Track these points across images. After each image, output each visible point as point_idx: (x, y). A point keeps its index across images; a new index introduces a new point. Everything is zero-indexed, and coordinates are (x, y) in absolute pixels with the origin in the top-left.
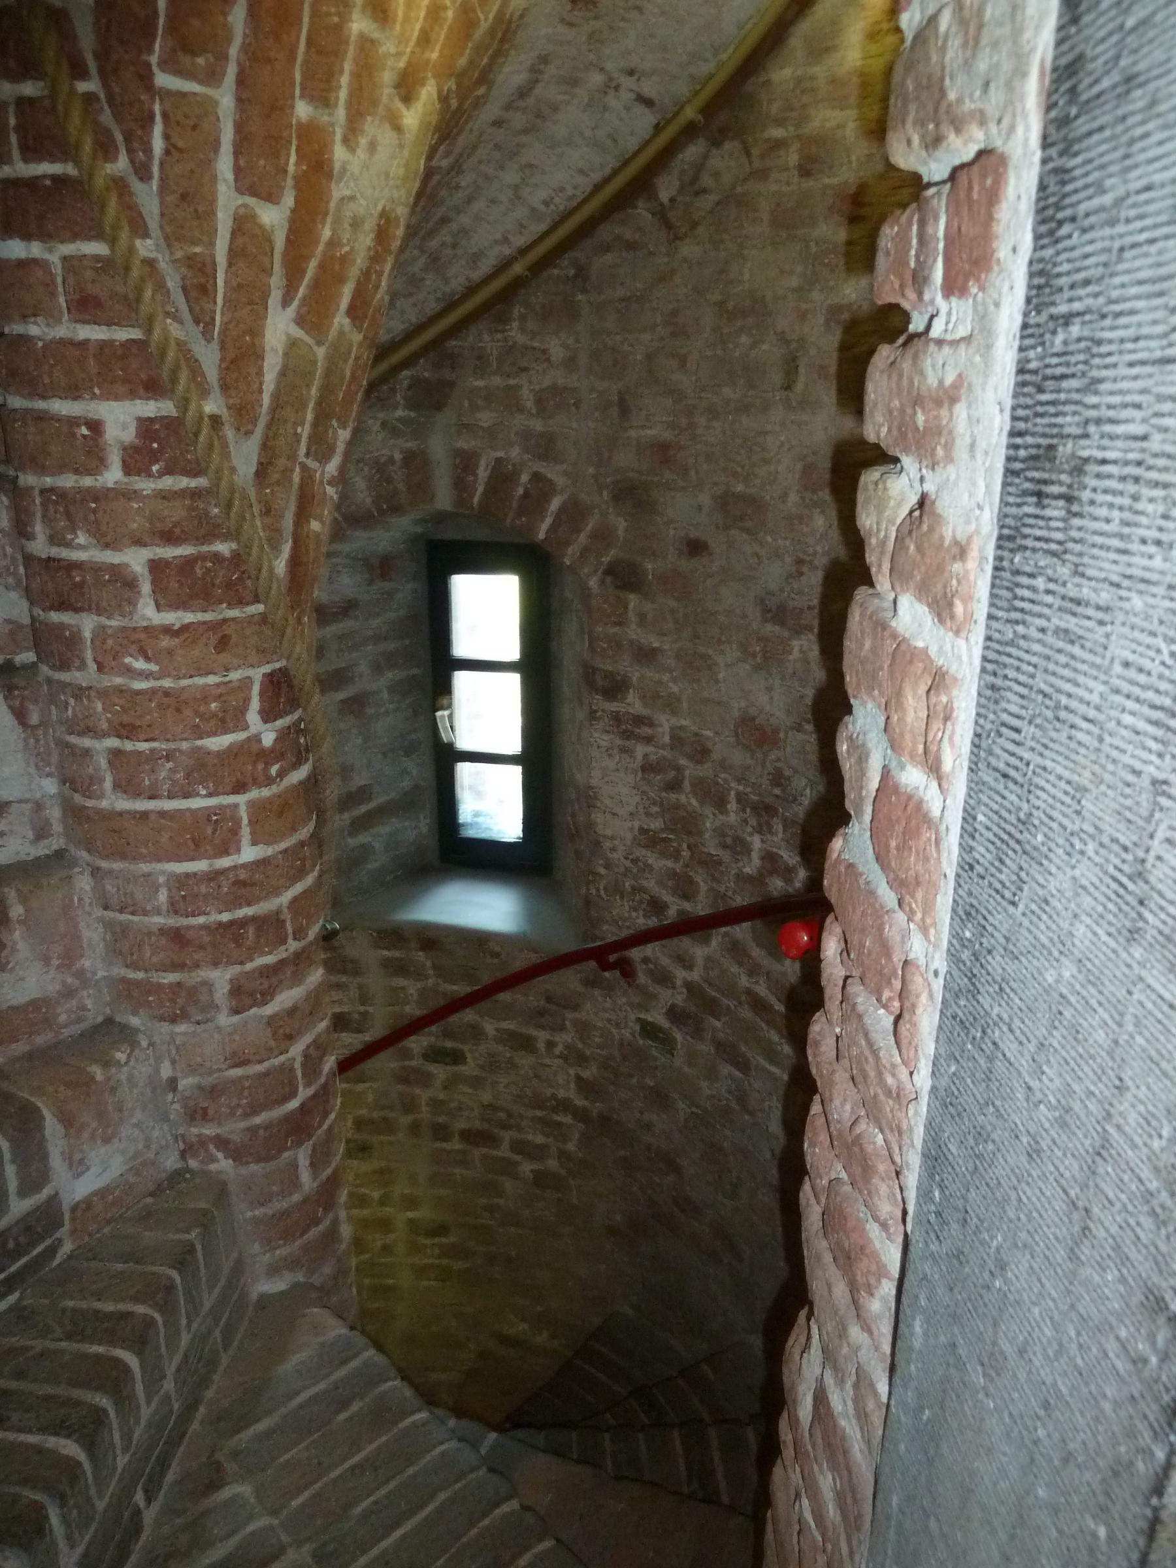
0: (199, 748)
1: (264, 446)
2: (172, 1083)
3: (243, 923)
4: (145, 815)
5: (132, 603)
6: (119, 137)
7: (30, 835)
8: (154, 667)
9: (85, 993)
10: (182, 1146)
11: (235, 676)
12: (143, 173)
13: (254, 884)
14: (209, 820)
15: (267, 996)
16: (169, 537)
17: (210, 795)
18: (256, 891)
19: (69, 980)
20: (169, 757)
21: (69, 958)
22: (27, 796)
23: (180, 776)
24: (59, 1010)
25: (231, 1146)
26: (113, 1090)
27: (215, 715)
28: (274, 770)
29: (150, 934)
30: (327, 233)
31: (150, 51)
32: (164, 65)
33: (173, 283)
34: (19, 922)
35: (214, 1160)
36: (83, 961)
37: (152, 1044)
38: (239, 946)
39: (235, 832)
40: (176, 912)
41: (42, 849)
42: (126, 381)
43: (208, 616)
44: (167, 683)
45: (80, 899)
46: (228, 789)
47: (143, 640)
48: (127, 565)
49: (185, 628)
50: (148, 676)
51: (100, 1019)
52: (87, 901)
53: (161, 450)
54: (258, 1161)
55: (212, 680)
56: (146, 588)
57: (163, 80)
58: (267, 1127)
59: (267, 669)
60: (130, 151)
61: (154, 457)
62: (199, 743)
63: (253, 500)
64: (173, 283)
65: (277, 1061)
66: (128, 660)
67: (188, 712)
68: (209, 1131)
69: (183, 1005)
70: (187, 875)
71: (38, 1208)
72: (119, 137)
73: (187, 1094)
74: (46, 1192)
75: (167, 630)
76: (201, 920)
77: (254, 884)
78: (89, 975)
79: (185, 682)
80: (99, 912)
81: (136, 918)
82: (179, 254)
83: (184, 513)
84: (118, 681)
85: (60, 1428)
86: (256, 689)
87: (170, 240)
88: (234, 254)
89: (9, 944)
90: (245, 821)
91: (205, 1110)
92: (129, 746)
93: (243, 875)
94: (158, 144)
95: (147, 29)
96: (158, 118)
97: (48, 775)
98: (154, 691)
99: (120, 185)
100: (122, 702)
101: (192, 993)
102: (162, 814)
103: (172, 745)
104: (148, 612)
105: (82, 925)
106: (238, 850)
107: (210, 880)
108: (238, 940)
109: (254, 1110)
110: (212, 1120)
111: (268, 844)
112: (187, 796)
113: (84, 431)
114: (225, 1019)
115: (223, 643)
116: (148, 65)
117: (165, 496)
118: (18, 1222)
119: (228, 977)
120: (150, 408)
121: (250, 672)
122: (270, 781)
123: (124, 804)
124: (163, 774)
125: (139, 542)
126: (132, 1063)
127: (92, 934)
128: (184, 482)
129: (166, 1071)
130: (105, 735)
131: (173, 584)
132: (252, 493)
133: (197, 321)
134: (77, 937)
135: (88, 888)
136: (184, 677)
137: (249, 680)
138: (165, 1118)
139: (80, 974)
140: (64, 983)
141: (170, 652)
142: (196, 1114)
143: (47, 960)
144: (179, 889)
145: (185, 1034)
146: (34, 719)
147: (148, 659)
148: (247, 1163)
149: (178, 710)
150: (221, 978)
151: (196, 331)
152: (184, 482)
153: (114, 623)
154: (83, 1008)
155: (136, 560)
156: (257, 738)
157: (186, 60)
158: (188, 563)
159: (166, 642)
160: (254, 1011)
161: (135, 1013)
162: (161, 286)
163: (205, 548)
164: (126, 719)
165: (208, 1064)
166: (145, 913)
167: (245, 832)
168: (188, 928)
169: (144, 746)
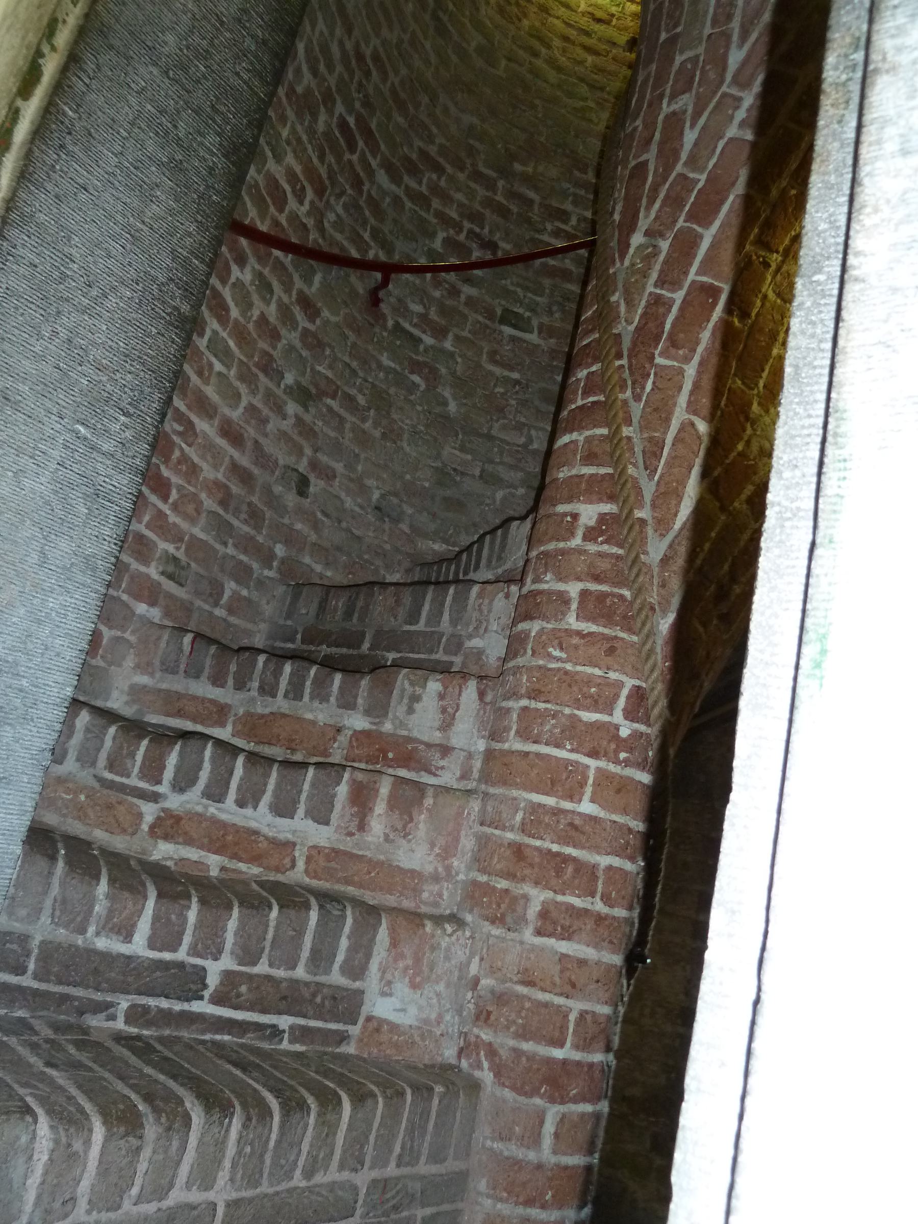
0: (575, 715)
1: (671, 546)
2: (476, 981)
3: (567, 859)
4: (527, 754)
5: (564, 614)
6: (629, 383)
7: (458, 774)
8: (564, 655)
9: (446, 884)
10: (462, 1043)
11: (613, 675)
12: (637, 398)
13: (583, 833)
14: (566, 768)
15: (567, 935)
16: (597, 579)
17: (572, 751)
18: (583, 839)
19: (440, 869)
20: (554, 716)
21: (447, 852)
22: (466, 748)
23: (558, 731)
24: (425, 887)
25: (497, 1060)
26: (433, 948)
27: (591, 696)
28: (623, 755)
29: (501, 845)
30: (740, 447)
31: (656, 347)
32: (661, 355)
33: (638, 449)
34: (428, 809)
35: (479, 1067)
36: (453, 860)
37: (472, 937)
38: (558, 876)
39: (582, 784)
40: (523, 831)
41: (462, 785)
42: (599, 493)
43: (606, 631)
44: (569, 667)
45: (469, 814)
46: (585, 751)
47: (562, 638)
48: (568, 592)
49: (590, 634)
50: (559, 659)
51: (448, 912)
52: (473, 818)
53: (606, 530)
54: (514, 1088)
55: (597, 672)
56: (574, 606)
57: (659, 360)
58: (531, 1057)
59: (637, 683)
60: (633, 388)
61: (602, 533)
62: (576, 712)
63: (655, 574)
64: (638, 449)
65: (560, 1000)
66: (551, 650)
67: (575, 689)
68: (486, 1035)
69: (504, 911)
70: (540, 805)
71: (347, 990)
72: (629, 383)
73: (482, 993)
74: (357, 985)
75: (579, 633)
76: (538, 843)
77: (583, 833)
78: (454, 873)
79: (579, 668)
80: (477, 828)
81: (497, 832)
82: (646, 435)
83: (609, 566)
84: (541, 662)
85: (277, 1093)
86: (625, 692)
87: (641, 429)
88: (677, 440)
89: (415, 821)
90: (590, 781)
91: (489, 1013)
92: (533, 704)
93: (578, 821)
94: (649, 386)
95: (657, 338)
96: (652, 376)
97: (483, 737)
98: (559, 669)
99: (625, 402)
100: (538, 675)
101: (514, 900)
102: (538, 755)
103: (558, 708)
104: (572, 621)
105: (463, 833)
106: (580, 801)
107: (554, 814)
108: (559, 872)
109: (524, 1034)
110: (491, 1026)
111: (603, 807)
112: (557, 746)
113: (569, 519)
114: (528, 936)
115: (611, 651)
116: (654, 354)
117: (600, 555)
118: (330, 986)
119: (542, 898)
120: (607, 508)
121: (624, 678)
122: (617, 762)
123: (519, 746)
124: (548, 727)
125: (579, 579)
126: (454, 938)
127: (467, 843)
128: (615, 550)
129: (474, 969)
130: (521, 697)
131: (591, 606)
132: (656, 570)
133: (646, 469)
134: (457, 840)
135: (477, 809)
136: (580, 664)
137: (620, 685)
138: (459, 1012)
139: (448, 868)
140: (436, 869)
141: (576, 647)
142: (482, 1016)
143: (432, 845)
144: (531, 814)
145: (497, 937)
146: (489, 698)
147: (562, 649)
148: (503, 1085)
149: (570, 686)
150: (538, 897)
151: (645, 474)
152: (615, 550)
153: (550, 626)
154: (440, 895)
155: (574, 589)
156: (617, 727)
157: (673, 351)
158: (602, 596)
159: (575, 640)
160: (552, 941)
161: (471, 911)
162: (631, 449)
163: (616, 590)
164: (537, 686)
165: (504, 971)
166: (504, 828)
167: (589, 790)
168: (528, 846)
169: (541, 706)
